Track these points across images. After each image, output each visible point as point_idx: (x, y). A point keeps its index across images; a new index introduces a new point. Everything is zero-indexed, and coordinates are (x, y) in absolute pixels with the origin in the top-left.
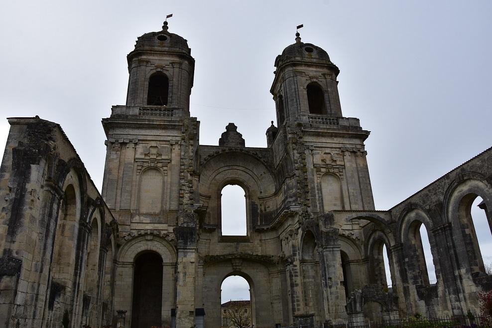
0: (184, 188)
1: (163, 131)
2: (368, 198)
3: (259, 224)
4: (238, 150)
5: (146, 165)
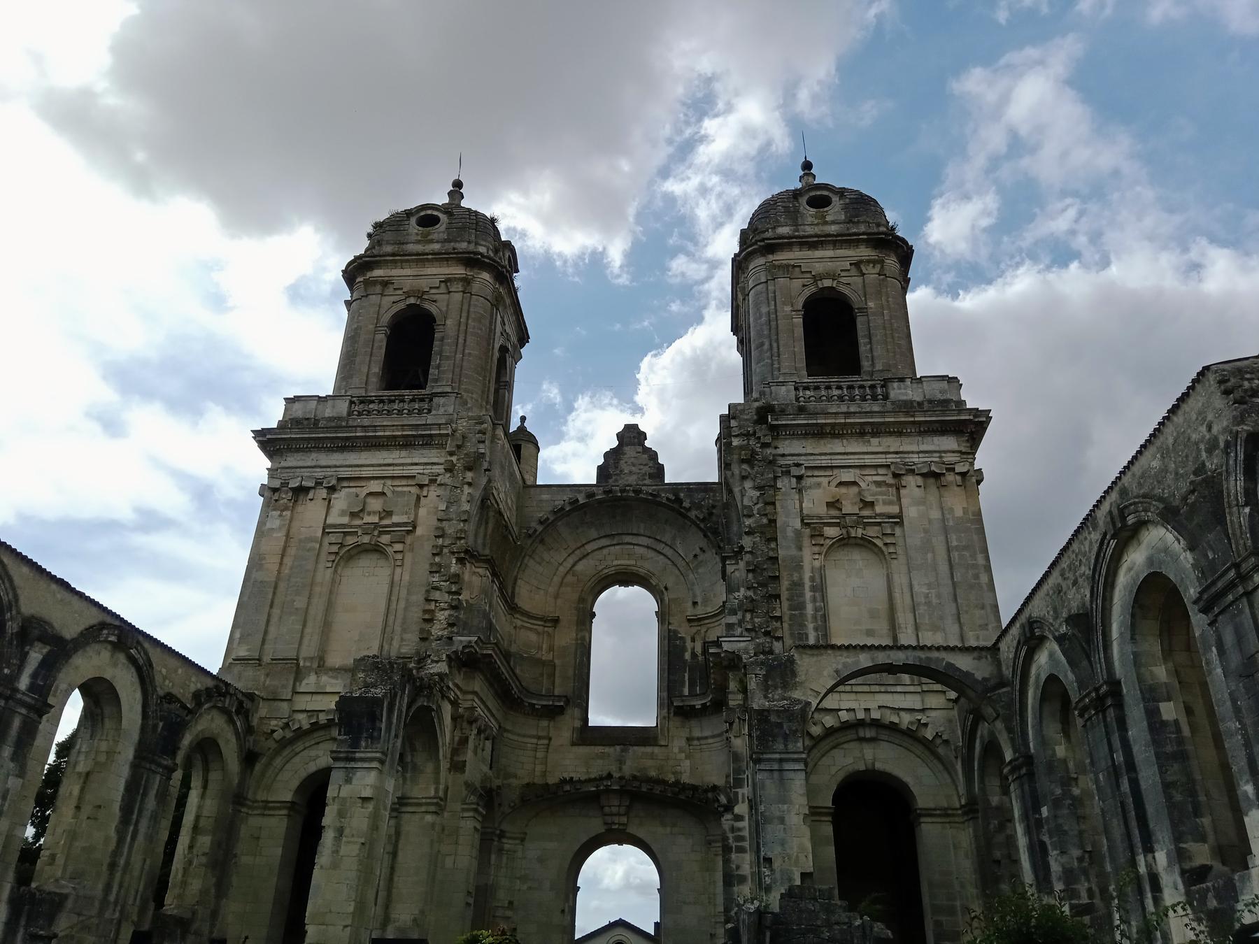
0: (436, 595)
1: (404, 453)
2: (978, 613)
3: (686, 691)
4: (628, 491)
5: (350, 540)
